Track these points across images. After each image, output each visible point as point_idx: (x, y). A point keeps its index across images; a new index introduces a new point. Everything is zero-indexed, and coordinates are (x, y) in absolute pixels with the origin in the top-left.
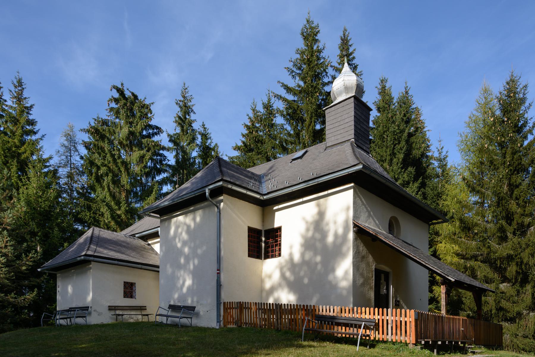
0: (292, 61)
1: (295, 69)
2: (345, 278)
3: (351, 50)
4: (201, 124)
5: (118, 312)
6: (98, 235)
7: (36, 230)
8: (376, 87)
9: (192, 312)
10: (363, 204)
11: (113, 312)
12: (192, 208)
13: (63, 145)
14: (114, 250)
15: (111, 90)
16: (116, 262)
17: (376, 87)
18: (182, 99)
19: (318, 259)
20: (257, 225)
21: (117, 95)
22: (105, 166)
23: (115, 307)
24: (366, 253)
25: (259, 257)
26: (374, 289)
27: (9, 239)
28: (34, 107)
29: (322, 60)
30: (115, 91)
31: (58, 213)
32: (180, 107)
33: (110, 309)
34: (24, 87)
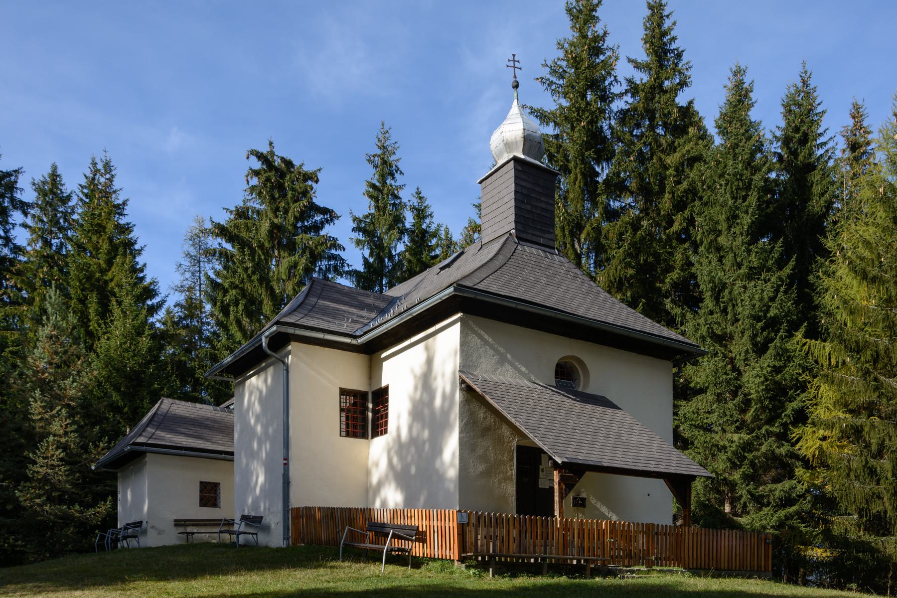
0: (547, 66)
1: (554, 79)
2: (452, 464)
3: (667, 24)
4: (414, 191)
5: (189, 529)
6: (166, 411)
7: (121, 404)
8: (725, 87)
9: (258, 525)
10: (486, 343)
11: (181, 529)
12: (264, 364)
13: (188, 255)
14: (185, 434)
15: (248, 158)
16: (183, 452)
17: (725, 87)
18: (379, 152)
19: (426, 434)
20: (357, 383)
21: (257, 165)
22: (236, 287)
23: (185, 521)
24: (494, 422)
25: (364, 436)
26: (515, 481)
27: (68, 421)
28: (128, 203)
29: (609, 53)
30: (253, 159)
31: (152, 374)
32: (376, 166)
33: (176, 525)
34: (113, 173)
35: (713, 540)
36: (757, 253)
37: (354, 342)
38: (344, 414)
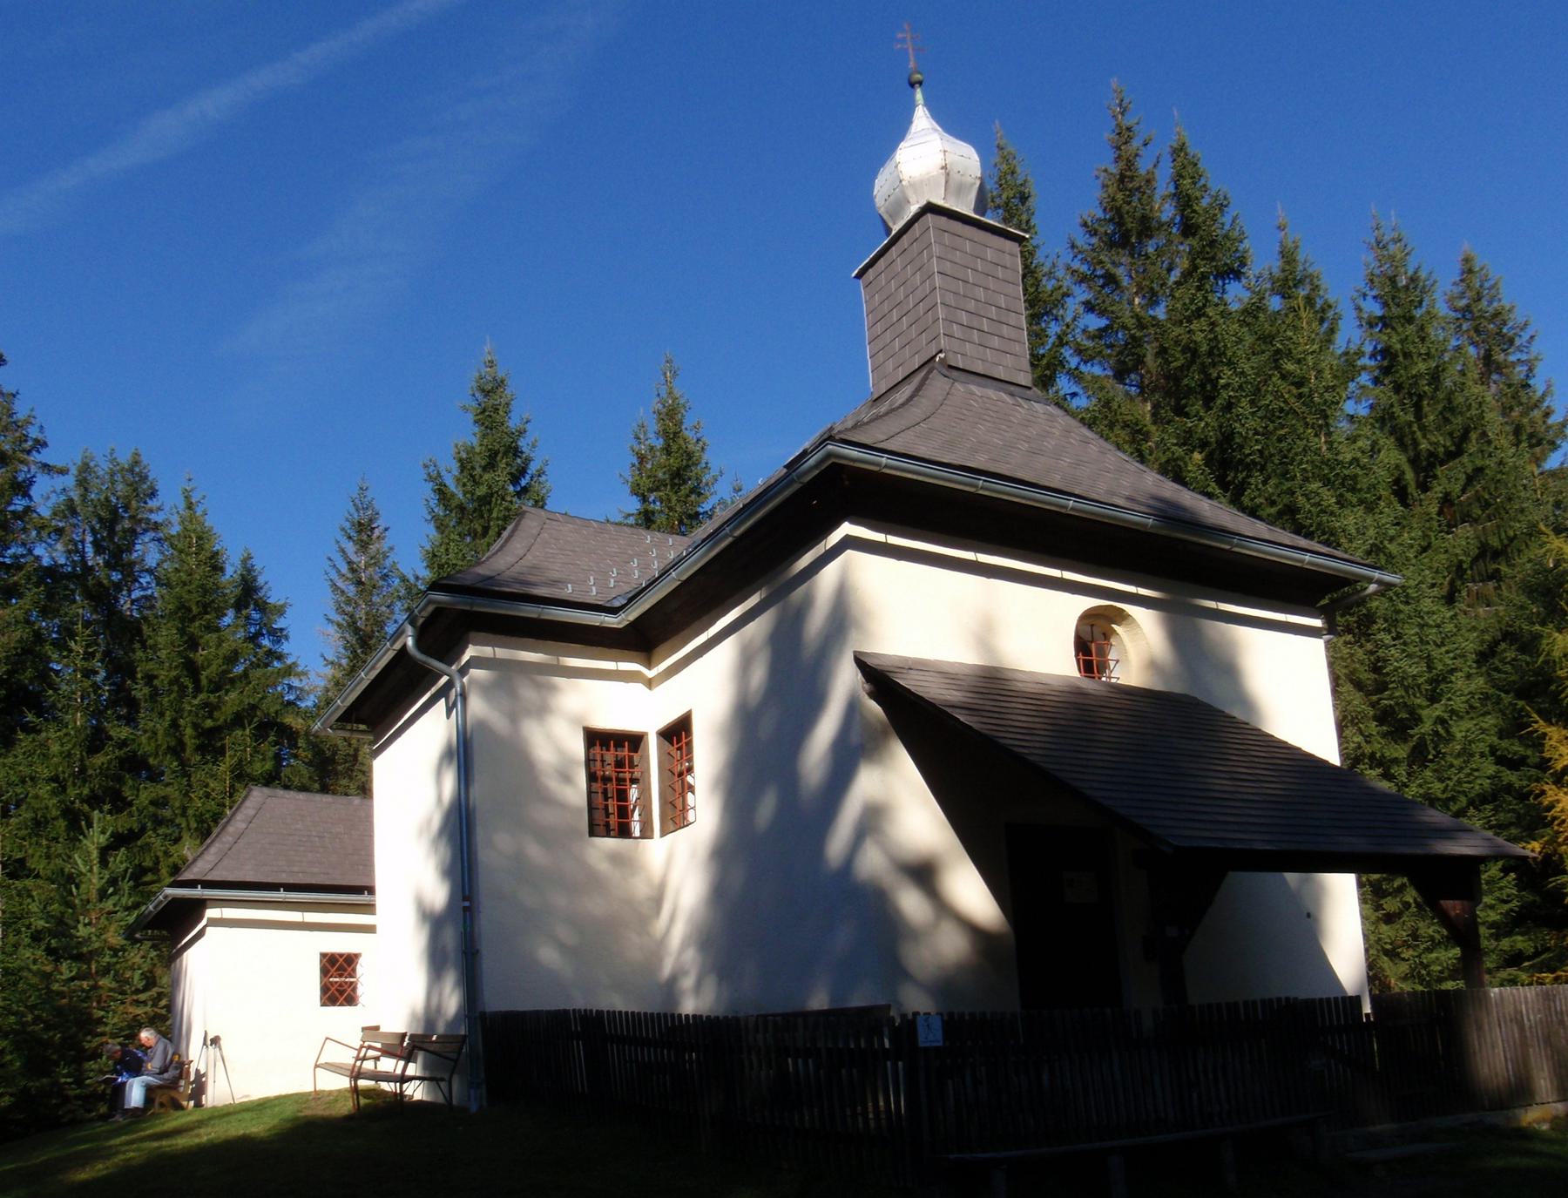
35: (1098, 754)
36: (47, 977)
37: (611, 621)
38: (597, 786)
